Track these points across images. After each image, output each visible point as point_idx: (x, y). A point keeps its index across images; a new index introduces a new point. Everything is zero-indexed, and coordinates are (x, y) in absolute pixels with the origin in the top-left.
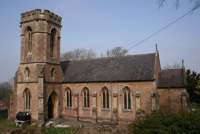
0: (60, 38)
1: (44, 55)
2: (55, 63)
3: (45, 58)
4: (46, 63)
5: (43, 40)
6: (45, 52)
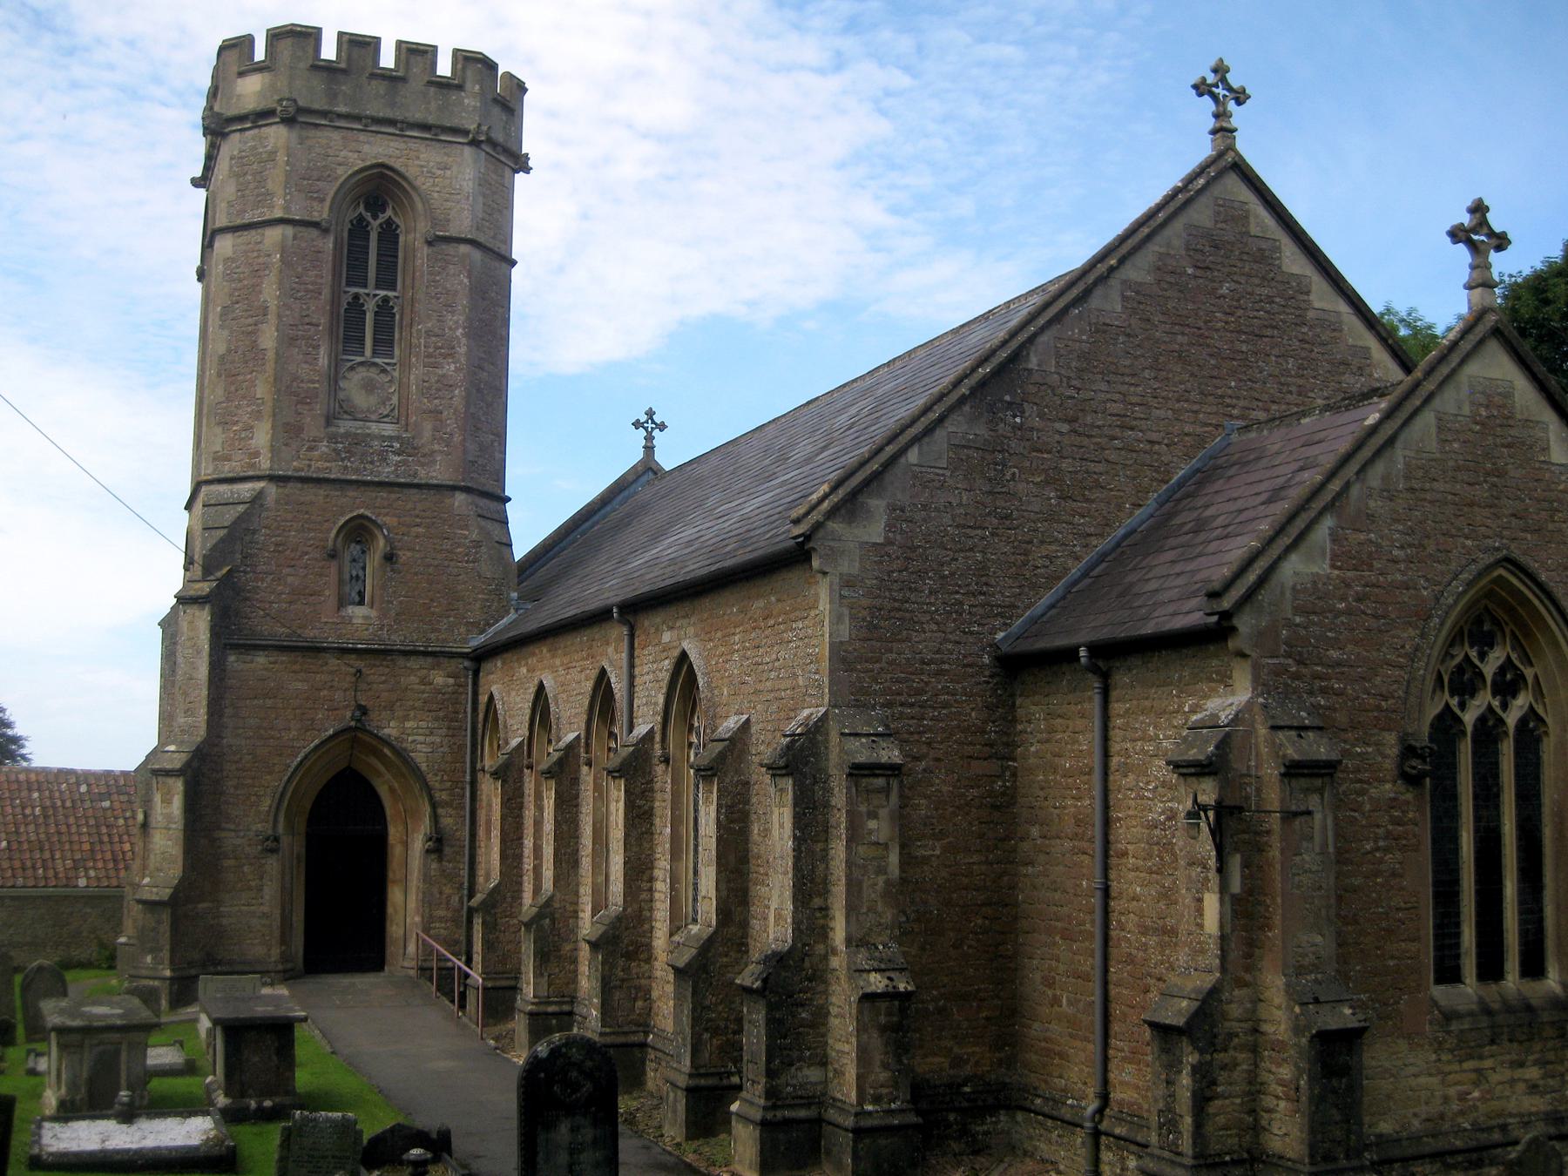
0: (514, 263)
1: (258, 415)
2: (386, 473)
3: (262, 437)
4: (271, 478)
5: (256, 289)
6: (262, 390)
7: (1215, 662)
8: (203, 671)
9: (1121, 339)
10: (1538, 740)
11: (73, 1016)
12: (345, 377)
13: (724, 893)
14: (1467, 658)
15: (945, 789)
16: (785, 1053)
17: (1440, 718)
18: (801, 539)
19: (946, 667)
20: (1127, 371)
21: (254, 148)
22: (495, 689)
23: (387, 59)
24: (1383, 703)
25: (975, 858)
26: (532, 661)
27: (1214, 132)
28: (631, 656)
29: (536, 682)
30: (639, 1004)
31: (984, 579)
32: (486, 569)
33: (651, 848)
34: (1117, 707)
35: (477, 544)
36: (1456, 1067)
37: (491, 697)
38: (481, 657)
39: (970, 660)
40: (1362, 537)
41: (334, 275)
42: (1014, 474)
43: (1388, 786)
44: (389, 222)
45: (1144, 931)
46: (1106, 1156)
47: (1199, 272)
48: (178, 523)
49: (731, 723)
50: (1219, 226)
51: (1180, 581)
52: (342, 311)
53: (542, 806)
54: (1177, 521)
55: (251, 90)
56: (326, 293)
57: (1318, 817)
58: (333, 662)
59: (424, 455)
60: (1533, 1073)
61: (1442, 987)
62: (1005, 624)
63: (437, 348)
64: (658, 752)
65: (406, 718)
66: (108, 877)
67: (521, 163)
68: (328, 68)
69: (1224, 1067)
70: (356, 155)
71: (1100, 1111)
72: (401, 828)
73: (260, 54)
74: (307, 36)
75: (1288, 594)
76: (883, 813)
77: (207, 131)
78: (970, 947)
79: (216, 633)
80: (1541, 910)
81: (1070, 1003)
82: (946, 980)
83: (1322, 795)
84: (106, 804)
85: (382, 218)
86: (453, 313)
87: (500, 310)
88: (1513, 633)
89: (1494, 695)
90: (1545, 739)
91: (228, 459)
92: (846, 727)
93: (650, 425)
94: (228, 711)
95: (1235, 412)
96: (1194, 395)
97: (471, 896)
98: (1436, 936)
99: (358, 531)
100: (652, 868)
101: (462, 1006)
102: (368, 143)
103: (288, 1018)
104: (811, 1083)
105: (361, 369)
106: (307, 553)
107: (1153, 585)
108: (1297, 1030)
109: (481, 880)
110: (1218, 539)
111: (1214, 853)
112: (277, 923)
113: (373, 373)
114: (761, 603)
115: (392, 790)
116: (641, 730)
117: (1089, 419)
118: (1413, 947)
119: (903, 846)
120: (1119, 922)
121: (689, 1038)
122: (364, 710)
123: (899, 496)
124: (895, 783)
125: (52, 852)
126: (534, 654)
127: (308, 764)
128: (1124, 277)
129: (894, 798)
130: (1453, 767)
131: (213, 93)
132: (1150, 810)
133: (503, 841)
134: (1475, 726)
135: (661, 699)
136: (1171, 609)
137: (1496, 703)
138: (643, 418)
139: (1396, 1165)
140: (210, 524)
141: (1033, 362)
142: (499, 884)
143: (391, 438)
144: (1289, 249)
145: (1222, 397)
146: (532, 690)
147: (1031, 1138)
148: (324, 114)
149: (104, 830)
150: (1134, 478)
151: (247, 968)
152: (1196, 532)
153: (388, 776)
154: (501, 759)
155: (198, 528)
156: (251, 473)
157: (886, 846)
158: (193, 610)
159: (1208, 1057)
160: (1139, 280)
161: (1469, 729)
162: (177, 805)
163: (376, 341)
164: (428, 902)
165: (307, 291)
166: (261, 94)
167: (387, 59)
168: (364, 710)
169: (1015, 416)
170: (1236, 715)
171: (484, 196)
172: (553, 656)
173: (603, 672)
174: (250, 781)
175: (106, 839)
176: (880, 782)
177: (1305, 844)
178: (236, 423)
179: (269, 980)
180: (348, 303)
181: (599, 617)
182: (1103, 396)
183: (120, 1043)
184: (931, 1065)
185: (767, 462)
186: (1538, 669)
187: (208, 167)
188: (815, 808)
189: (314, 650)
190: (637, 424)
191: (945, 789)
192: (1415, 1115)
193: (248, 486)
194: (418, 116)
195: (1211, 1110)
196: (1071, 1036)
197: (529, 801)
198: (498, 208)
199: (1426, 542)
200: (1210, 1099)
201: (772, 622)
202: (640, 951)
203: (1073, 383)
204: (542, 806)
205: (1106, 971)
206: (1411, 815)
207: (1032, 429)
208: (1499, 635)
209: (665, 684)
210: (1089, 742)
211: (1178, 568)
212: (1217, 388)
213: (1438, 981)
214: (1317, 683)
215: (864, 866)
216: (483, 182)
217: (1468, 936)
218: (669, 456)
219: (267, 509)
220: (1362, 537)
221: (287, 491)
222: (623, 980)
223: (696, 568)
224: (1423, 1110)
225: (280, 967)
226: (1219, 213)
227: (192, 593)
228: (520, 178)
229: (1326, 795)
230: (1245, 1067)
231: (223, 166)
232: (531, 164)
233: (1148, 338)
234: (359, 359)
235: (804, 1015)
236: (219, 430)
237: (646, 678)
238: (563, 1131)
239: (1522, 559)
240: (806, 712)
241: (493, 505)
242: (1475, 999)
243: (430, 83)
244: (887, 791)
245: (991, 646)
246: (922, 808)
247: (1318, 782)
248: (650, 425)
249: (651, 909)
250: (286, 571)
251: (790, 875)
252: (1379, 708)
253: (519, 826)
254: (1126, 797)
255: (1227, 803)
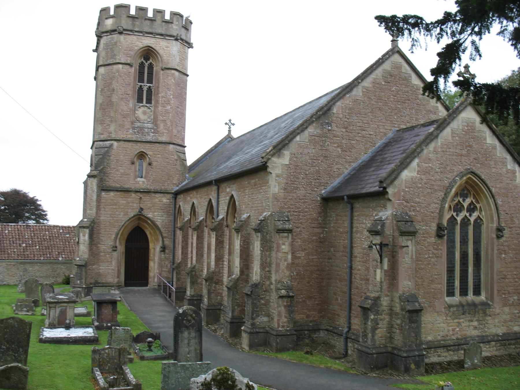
2: (149, 138)
7: (382, 202)
8: (95, 197)
9: (362, 104)
10: (480, 226)
11: (53, 299)
12: (137, 110)
13: (242, 266)
14: (459, 201)
15: (306, 236)
16: (257, 313)
17: (450, 219)
18: (264, 163)
19: (307, 201)
20: (363, 113)
21: (110, 41)
22: (181, 204)
23: (150, 14)
24: (432, 214)
25: (315, 257)
26: (191, 195)
27: (392, 41)
28: (218, 195)
29: (192, 202)
30: (219, 297)
31: (319, 175)
32: (179, 167)
33: (223, 252)
34: (355, 214)
35: (176, 160)
36: (452, 321)
37: (180, 206)
38: (176, 194)
39: (314, 199)
40: (427, 165)
41: (134, 80)
42: (328, 144)
43: (433, 239)
44: (151, 64)
45: (362, 280)
46: (350, 345)
47: (386, 84)
48: (89, 153)
49: (245, 216)
50: (393, 70)
51: (375, 177)
52: (137, 90)
53: (193, 239)
54: (377, 158)
55: (109, 23)
56: (132, 84)
57: (410, 247)
58: (133, 195)
59: (161, 134)
60: (475, 323)
61: (449, 298)
62: (325, 188)
63: (165, 101)
64: (225, 224)
65: (155, 212)
66: (68, 257)
67: (190, 45)
68: (133, 17)
69: (381, 320)
70: (141, 43)
71: (348, 332)
72: (153, 244)
73: (112, 13)
74: (127, 7)
75: (404, 182)
76: (287, 243)
77: (97, 36)
78: (313, 283)
79: (98, 186)
80: (480, 276)
81: (341, 300)
82: (305, 292)
83: (412, 241)
84: (68, 236)
85: (149, 62)
86: (169, 91)
87: (184, 90)
88: (473, 194)
89: (467, 212)
90: (483, 225)
91: (102, 134)
92: (276, 218)
93: (230, 124)
94: (103, 209)
95: (396, 126)
96: (384, 121)
97: (173, 265)
98: (447, 283)
99: (142, 156)
100: (223, 258)
101: (170, 297)
102: (144, 40)
103: (116, 300)
104: (265, 322)
105: (142, 108)
106: (125, 163)
107: (367, 178)
108: (402, 309)
109: (176, 260)
110: (387, 164)
111: (379, 258)
112: (116, 272)
113: (146, 109)
114: (253, 181)
115: (150, 233)
116: (221, 217)
117: (351, 128)
118: (439, 286)
119: (292, 253)
120: (354, 276)
121: (231, 308)
122: (142, 209)
123: (294, 150)
124: (290, 235)
125: (52, 250)
126: (192, 194)
127: (125, 225)
128: (363, 85)
129: (290, 239)
130: (454, 233)
131: (99, 24)
132: (364, 244)
133: (182, 249)
134: (461, 221)
135: (226, 208)
136: (370, 185)
137: (468, 215)
138: (228, 122)
139: (433, 349)
140: (97, 154)
141: (335, 110)
142: (181, 261)
143: (151, 128)
144: (414, 76)
145: (392, 121)
146: (191, 204)
147: (329, 339)
148: (131, 31)
149: (67, 243)
150: (365, 145)
151: (107, 285)
152: (381, 162)
153: (149, 229)
154: (182, 224)
155: (94, 154)
156: (109, 139)
157: (287, 253)
158: (92, 179)
159: (376, 317)
160: (368, 86)
161: (459, 222)
162: (87, 237)
163: (147, 99)
164: (160, 266)
165: (126, 84)
166: (112, 25)
167: (150, 14)
168: (142, 209)
169: (329, 127)
170: (387, 218)
171: (179, 55)
172: (197, 194)
173: (210, 200)
174: (108, 230)
175: (68, 246)
176: (286, 234)
177: (406, 255)
178: (105, 124)
179: (114, 289)
180: (139, 88)
181: (208, 184)
182: (356, 121)
183: (66, 307)
184: (299, 317)
185: (261, 137)
186: (480, 205)
187: (97, 46)
188: (267, 242)
189: (127, 191)
190: (226, 124)
191: (306, 236)
192: (439, 335)
193: (108, 142)
194: (159, 31)
195: (377, 332)
196: (341, 309)
197: (190, 237)
198: (184, 58)
199: (447, 167)
200: (376, 329)
201: (256, 187)
202: (219, 282)
203: (347, 117)
204: (193, 239)
205: (350, 290)
206: (440, 247)
207: (334, 130)
208: (469, 194)
209: (227, 204)
210: (347, 224)
211: (375, 173)
212: (390, 118)
213: (447, 296)
214: (412, 208)
215: (281, 259)
216: (179, 52)
217: (457, 283)
218: (235, 134)
219: (114, 150)
220: (427, 165)
221: (120, 144)
222: (214, 290)
223: (236, 170)
224: (441, 334)
225: (117, 285)
226: (393, 66)
227: (92, 174)
228: (190, 49)
229: (413, 241)
230: (387, 320)
231: (101, 46)
232: (193, 45)
233: (370, 104)
234: (143, 105)
235: (263, 302)
236: (100, 126)
237: (223, 202)
238: (186, 334)
239: (478, 172)
240: (265, 214)
241: (181, 148)
242: (458, 301)
243: (163, 21)
244: (288, 237)
245: (320, 195)
246: (299, 242)
247: (411, 237)
248: (230, 124)
249: (223, 270)
250: (120, 168)
251: (259, 261)
252: (430, 215)
253: (187, 244)
254: (357, 240)
255: (383, 243)
